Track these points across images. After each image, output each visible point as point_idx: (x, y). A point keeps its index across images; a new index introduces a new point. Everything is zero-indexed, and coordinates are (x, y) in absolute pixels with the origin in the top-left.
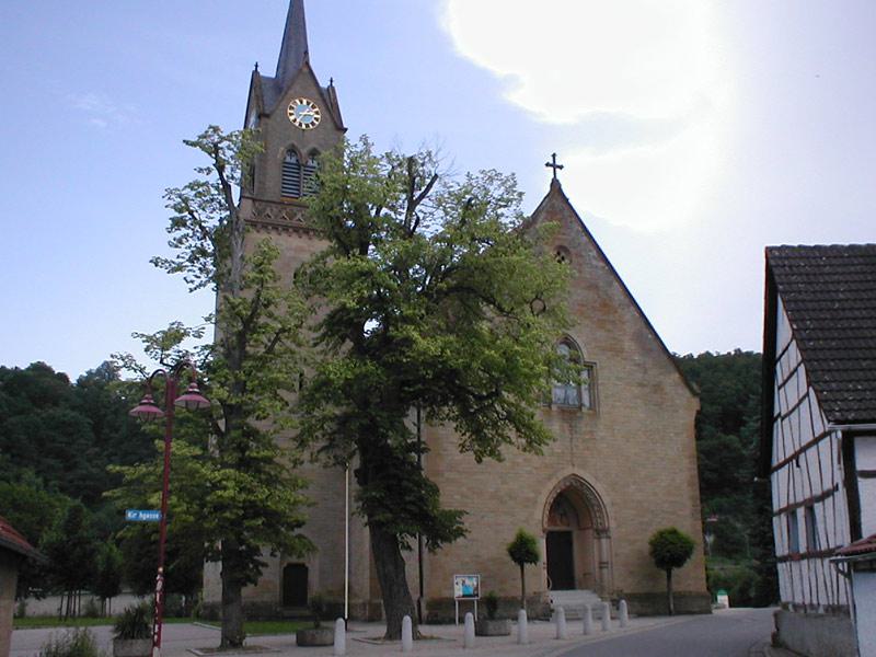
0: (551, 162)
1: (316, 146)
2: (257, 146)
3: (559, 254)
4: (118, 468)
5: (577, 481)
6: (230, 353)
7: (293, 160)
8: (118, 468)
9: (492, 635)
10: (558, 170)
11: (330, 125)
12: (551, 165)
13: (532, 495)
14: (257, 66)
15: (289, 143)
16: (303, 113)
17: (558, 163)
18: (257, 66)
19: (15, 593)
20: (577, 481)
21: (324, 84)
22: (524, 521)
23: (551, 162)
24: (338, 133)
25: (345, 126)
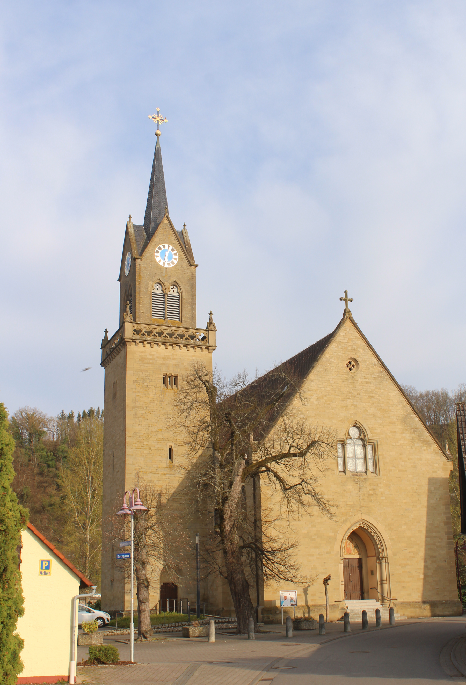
0: (344, 297)
1: (175, 279)
2: (117, 574)
3: (350, 363)
4: (88, 567)
5: (364, 523)
6: (122, 343)
7: (160, 291)
8: (88, 567)
9: (304, 630)
10: (349, 302)
11: (186, 263)
12: (344, 300)
13: (332, 534)
14: (130, 217)
15: (157, 277)
16: (164, 256)
17: (349, 297)
18: (130, 217)
19: (435, 598)
20: (364, 523)
21: (179, 228)
22: (327, 553)
23: (344, 297)
24: (192, 268)
25: (196, 263)
